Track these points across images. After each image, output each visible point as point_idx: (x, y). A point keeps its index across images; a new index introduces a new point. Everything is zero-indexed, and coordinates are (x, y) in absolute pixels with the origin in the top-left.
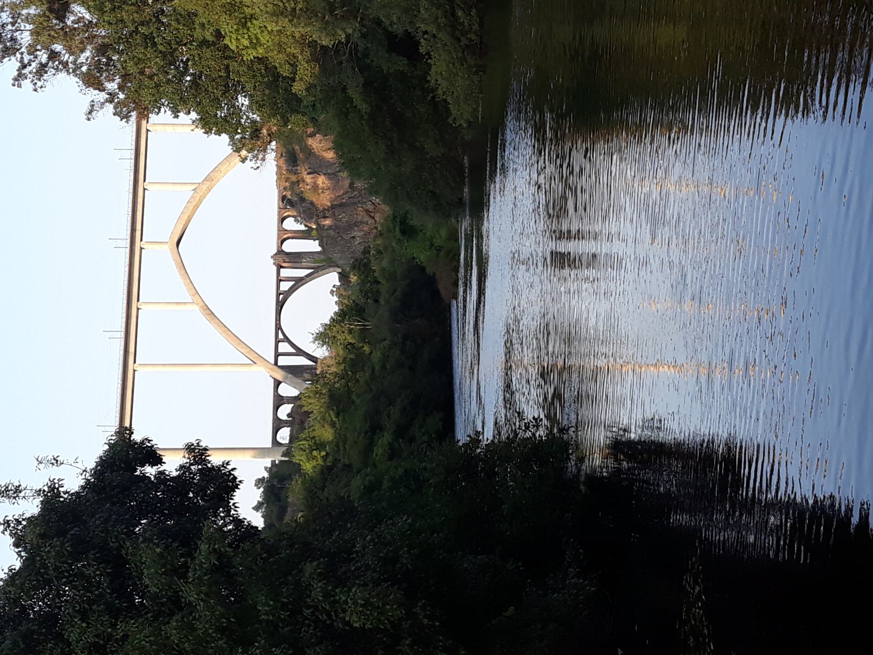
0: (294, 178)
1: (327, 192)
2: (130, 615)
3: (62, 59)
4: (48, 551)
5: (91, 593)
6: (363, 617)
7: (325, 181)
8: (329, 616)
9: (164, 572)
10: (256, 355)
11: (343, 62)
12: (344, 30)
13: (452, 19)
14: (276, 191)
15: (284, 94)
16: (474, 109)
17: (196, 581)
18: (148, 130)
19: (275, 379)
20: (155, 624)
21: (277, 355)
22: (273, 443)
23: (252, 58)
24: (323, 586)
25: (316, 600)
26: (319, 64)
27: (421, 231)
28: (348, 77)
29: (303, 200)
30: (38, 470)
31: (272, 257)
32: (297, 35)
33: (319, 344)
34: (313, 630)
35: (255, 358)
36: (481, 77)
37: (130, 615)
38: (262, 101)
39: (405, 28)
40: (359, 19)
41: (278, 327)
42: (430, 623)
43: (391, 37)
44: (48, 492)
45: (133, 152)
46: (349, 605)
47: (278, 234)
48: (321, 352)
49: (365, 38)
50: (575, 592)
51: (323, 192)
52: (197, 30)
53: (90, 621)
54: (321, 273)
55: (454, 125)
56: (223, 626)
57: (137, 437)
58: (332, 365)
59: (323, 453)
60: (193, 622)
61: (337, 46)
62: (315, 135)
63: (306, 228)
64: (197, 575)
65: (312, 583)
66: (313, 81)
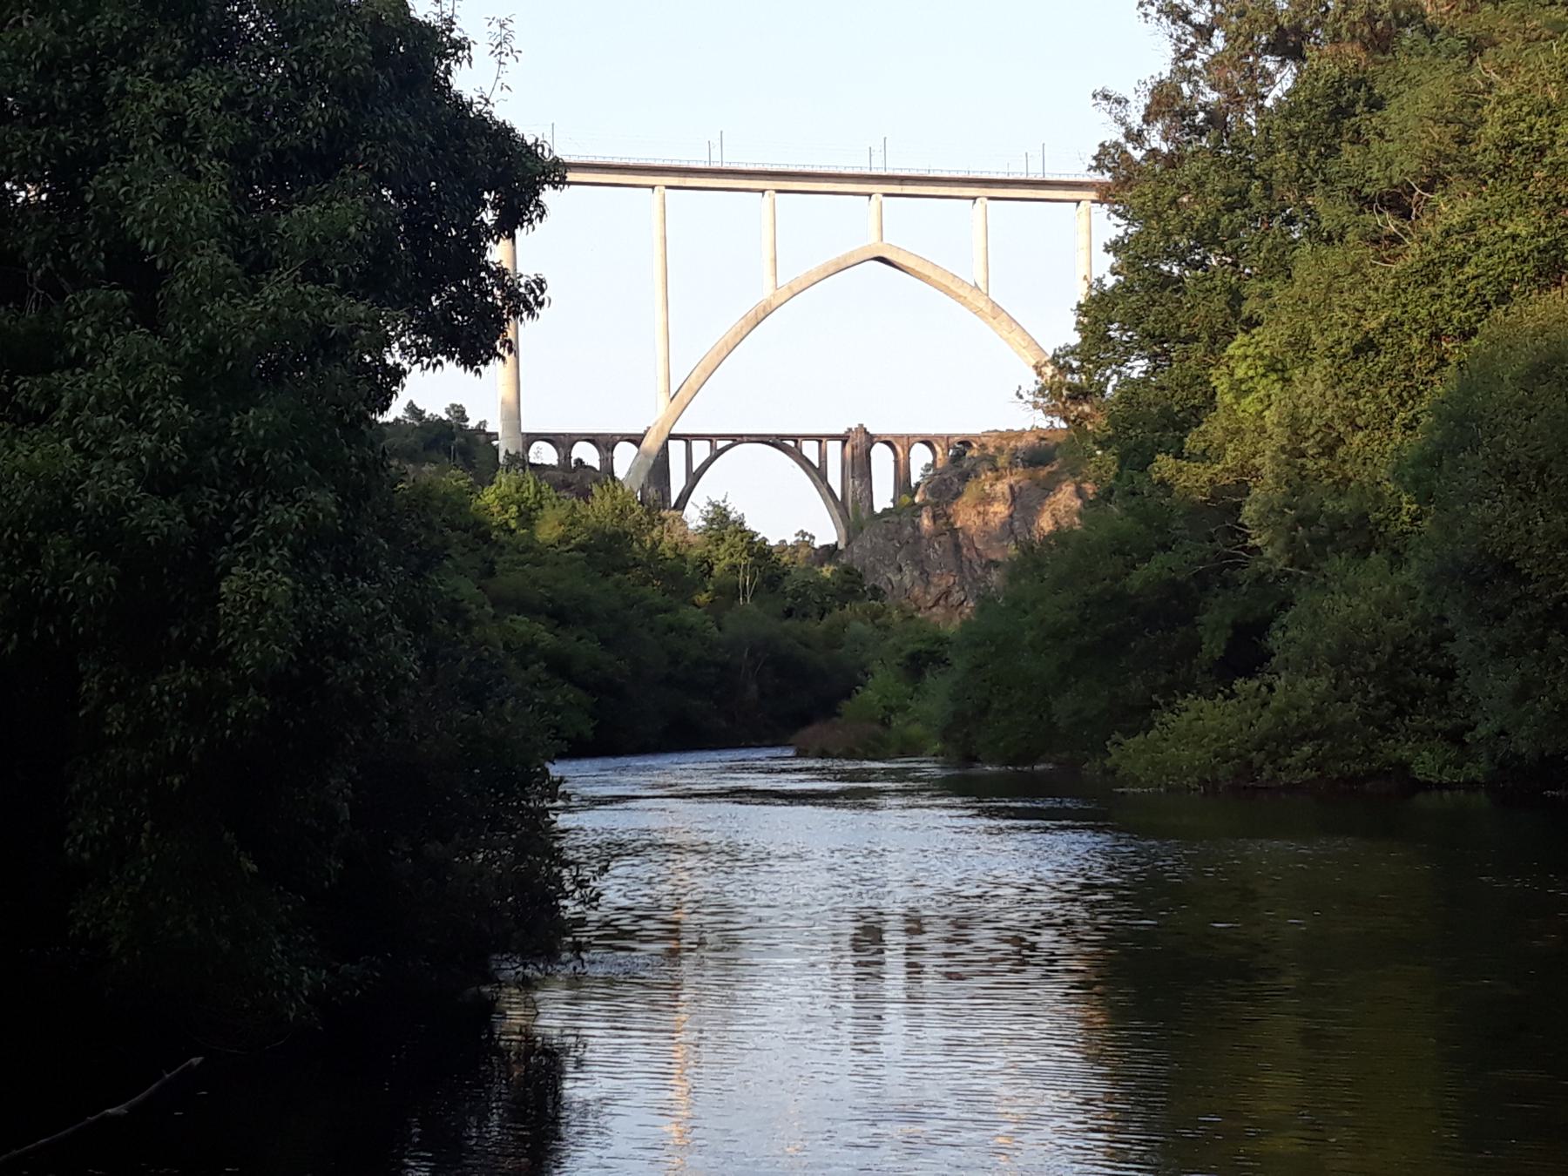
0: (1002, 461)
1: (979, 521)
2: (236, 183)
3: (1200, 49)
4: (348, 36)
5: (274, 115)
6: (238, 598)
7: (1000, 516)
8: (238, 538)
9: (314, 240)
10: (686, 401)
11: (1214, 544)
12: (1270, 543)
13: (1296, 735)
14: (978, 431)
15: (1153, 440)
16: (1138, 778)
17: (299, 298)
18: (1078, 202)
19: (643, 436)
20: (219, 228)
21: (688, 438)
22: (528, 434)
23: (1213, 385)
24: (294, 526)
25: (267, 513)
26: (1207, 501)
27: (916, 689)
28: (1186, 553)
29: (965, 477)
30: (489, 21)
31: (861, 425)
32: (1257, 461)
33: (708, 512)
34: (214, 507)
35: (681, 398)
36: (1195, 790)
37: (236, 183)
38: (1139, 403)
39: (1276, 651)
40: (1288, 569)
41: (737, 439)
42: (229, 720)
43: (1262, 627)
44: (449, 37)
45: (1039, 177)
46: (260, 574)
47: (902, 436)
48: (694, 515)
49: (1257, 580)
50: (286, 981)
51: (979, 513)
52: (1259, 285)
53: (223, 113)
54: (836, 512)
55: (1108, 743)
56: (218, 347)
57: (548, 195)
58: (672, 537)
59: (513, 524)
60: (225, 295)
61: (1241, 532)
62: (1081, 497)
63: (913, 485)
64: (309, 299)
65: (298, 505)
66: (1178, 492)
